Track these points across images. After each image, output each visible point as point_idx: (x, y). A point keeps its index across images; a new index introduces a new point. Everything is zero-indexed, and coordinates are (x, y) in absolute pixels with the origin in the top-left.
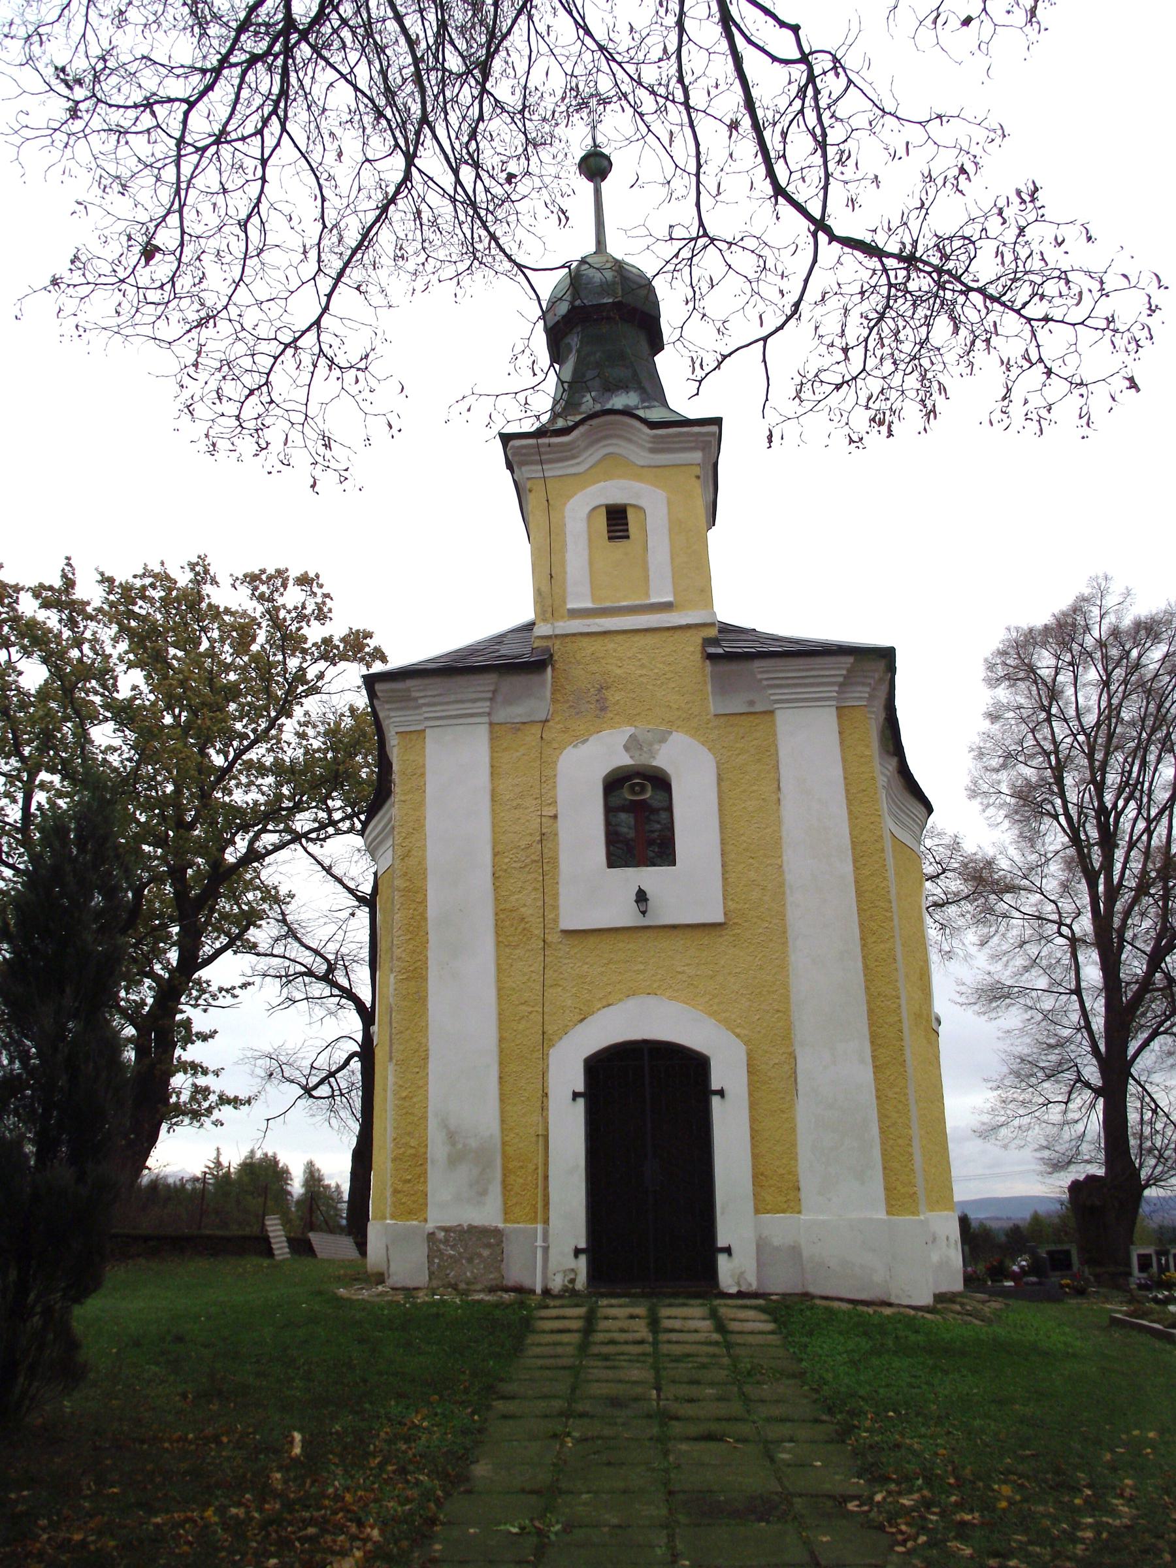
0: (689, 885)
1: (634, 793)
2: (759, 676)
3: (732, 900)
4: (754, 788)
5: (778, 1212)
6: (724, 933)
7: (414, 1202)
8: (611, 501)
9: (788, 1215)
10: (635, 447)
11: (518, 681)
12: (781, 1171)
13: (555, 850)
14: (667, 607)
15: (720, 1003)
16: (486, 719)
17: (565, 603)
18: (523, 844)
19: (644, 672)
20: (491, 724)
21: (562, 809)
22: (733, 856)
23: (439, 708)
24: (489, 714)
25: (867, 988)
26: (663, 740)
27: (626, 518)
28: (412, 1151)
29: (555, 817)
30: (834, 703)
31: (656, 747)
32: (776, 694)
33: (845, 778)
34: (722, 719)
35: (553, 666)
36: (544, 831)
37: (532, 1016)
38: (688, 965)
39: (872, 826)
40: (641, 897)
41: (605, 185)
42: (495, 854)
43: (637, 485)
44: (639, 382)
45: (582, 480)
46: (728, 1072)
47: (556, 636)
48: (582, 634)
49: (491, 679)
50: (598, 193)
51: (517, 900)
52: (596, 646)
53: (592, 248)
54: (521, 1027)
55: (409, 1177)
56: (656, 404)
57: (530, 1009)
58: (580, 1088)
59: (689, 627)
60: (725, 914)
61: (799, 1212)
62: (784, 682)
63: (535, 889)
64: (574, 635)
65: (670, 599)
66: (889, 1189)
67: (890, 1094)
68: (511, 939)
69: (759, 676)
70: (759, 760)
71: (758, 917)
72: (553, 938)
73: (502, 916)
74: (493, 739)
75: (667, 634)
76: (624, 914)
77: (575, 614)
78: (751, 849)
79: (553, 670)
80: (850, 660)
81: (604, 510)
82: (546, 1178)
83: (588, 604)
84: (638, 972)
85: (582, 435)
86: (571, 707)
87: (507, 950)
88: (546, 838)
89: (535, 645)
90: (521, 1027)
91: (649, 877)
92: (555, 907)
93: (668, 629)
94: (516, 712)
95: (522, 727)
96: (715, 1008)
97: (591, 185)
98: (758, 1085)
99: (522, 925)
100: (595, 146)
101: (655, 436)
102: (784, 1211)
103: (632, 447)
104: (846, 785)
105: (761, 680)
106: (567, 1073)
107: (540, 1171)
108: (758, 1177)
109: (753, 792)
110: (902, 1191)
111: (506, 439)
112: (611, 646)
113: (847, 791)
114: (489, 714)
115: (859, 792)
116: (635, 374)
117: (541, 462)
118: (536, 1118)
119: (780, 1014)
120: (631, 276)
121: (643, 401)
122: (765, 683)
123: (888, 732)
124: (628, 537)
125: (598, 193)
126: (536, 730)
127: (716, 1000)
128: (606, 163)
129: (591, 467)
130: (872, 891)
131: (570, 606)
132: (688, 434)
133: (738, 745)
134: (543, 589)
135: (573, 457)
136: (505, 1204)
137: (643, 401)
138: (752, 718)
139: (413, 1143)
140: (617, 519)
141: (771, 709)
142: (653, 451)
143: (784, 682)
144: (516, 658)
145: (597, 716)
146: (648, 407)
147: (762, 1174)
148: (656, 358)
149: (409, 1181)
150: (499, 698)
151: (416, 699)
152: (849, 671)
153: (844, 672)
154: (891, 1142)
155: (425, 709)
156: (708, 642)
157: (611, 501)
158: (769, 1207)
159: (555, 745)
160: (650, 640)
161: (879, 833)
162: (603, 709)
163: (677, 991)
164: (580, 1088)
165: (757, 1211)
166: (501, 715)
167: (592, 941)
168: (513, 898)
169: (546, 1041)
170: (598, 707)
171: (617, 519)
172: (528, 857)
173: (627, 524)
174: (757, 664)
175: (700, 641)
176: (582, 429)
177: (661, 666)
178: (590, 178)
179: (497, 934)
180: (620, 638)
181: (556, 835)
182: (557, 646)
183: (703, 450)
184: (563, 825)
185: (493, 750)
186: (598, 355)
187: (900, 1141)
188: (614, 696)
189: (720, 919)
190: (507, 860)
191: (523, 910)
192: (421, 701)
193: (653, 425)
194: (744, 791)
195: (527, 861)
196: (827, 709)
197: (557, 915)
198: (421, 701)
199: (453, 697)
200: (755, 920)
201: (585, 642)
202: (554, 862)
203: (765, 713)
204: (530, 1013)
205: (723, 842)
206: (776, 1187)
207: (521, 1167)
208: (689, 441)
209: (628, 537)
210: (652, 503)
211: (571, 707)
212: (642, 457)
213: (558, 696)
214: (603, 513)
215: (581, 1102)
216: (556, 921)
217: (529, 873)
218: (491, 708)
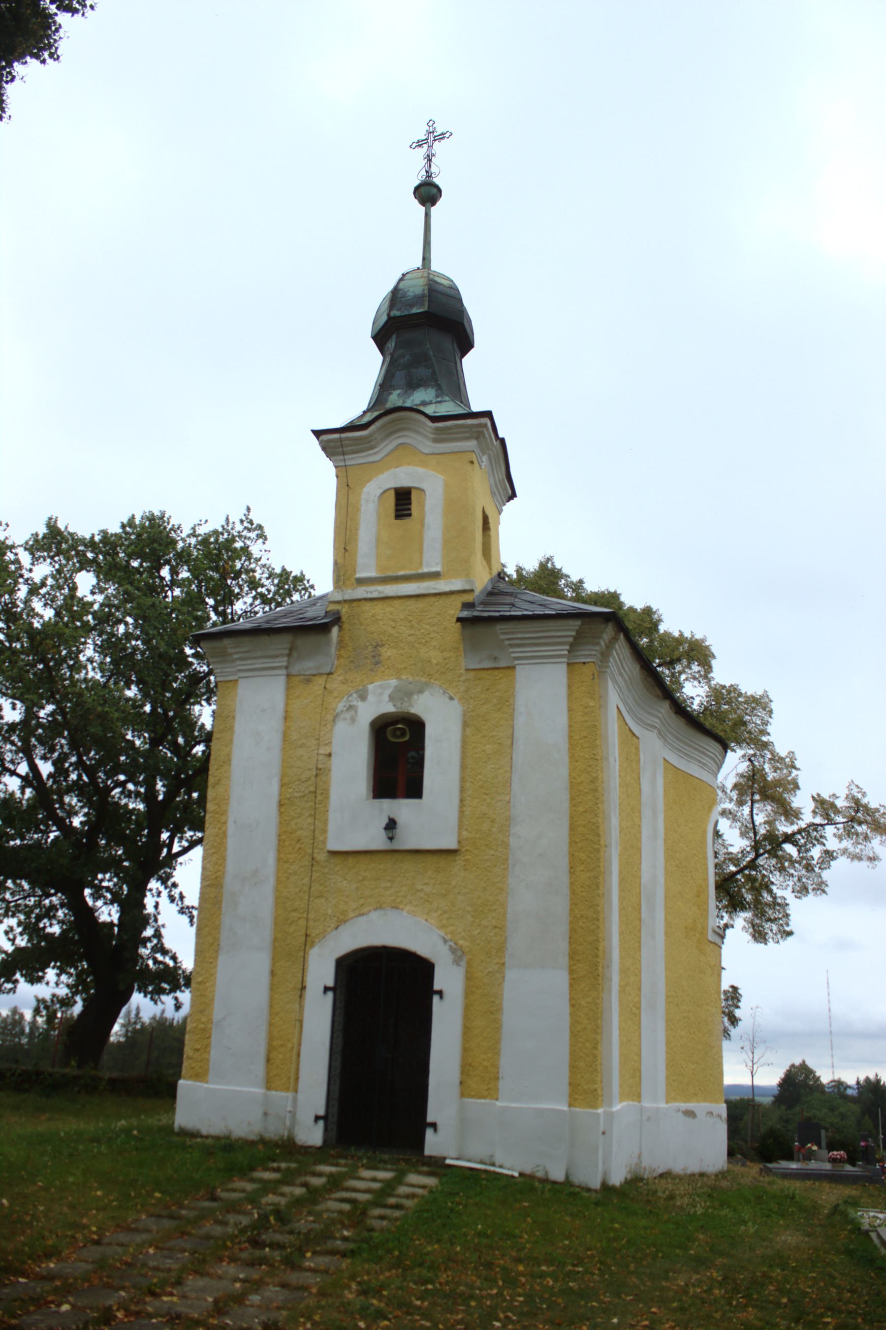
0: (432, 818)
1: (395, 736)
2: (502, 637)
3: (466, 830)
4: (494, 733)
5: (480, 1098)
6: (457, 858)
7: (201, 1067)
8: (399, 485)
9: (487, 1101)
10: (421, 439)
11: (305, 642)
12: (485, 1063)
13: (327, 783)
14: (435, 575)
15: (448, 919)
16: (284, 672)
17: (355, 572)
18: (303, 777)
19: (412, 632)
20: (288, 675)
21: (335, 749)
22: (469, 792)
23: (249, 662)
24: (287, 668)
25: (571, 910)
26: (421, 691)
27: (410, 499)
28: (202, 1026)
29: (330, 755)
30: (566, 660)
31: (415, 697)
32: (517, 652)
33: (570, 726)
34: (472, 674)
35: (340, 627)
36: (320, 766)
37: (300, 922)
38: (426, 884)
39: (589, 769)
40: (391, 825)
41: (433, 209)
42: (282, 785)
43: (421, 470)
44: (436, 381)
45: (377, 467)
46: (448, 978)
47: (345, 601)
48: (366, 599)
49: (285, 641)
50: (427, 216)
51: (296, 824)
52: (378, 609)
53: (419, 263)
54: (291, 930)
55: (198, 1047)
56: (447, 398)
57: (299, 915)
58: (331, 983)
59: (452, 593)
60: (459, 842)
61: (497, 1099)
62: (518, 642)
63: (310, 815)
64: (359, 600)
65: (438, 568)
66: (573, 1085)
67: (583, 1003)
68: (289, 856)
69: (502, 637)
70: (499, 710)
71: (486, 845)
72: (321, 857)
73: (284, 837)
74: (288, 688)
75: (433, 599)
76: (375, 839)
77: (361, 582)
78: (484, 785)
79: (340, 631)
80: (578, 623)
81: (392, 493)
82: (299, 1055)
83: (372, 573)
84: (387, 889)
85: (379, 429)
86: (352, 662)
87: (286, 866)
88: (321, 773)
89: (328, 609)
90: (291, 930)
91: (403, 809)
92: (324, 831)
93: (435, 595)
94: (307, 665)
95: (313, 678)
96: (444, 922)
97: (424, 208)
98: (474, 989)
99: (298, 845)
100: (429, 174)
101: (437, 429)
102: (485, 1097)
103: (420, 438)
104: (570, 732)
105: (503, 640)
106: (321, 971)
107: (295, 1050)
108: (466, 1067)
109: (493, 736)
110: (585, 1087)
111: (318, 433)
112: (389, 609)
113: (570, 737)
114: (287, 668)
115: (581, 739)
116: (434, 373)
117: (344, 454)
118: (297, 1006)
119: (497, 930)
120: (441, 288)
121: (437, 396)
122: (507, 642)
123: (650, 680)
124: (410, 515)
125: (427, 216)
126: (321, 681)
127: (446, 916)
128: (435, 191)
129: (387, 455)
130: (584, 826)
131: (358, 575)
132: (462, 426)
133: (483, 696)
134: (339, 561)
135: (372, 448)
136: (268, 1074)
137: (437, 396)
138: (496, 672)
139: (204, 1019)
140: (403, 501)
141: (509, 664)
142: (436, 441)
143: (518, 642)
144: (311, 620)
145: (371, 670)
146: (440, 402)
147: (470, 1065)
148: (464, 360)
149: (198, 1050)
150: (295, 654)
151: (231, 654)
152: (578, 632)
153: (574, 633)
154: (580, 1044)
155: (238, 663)
156: (467, 606)
157: (398, 485)
158: (473, 1093)
159: (335, 694)
160: (411, 603)
161: (594, 775)
162: (377, 663)
163: (416, 906)
164: (331, 983)
165: (462, 1095)
166: (297, 668)
167: (351, 860)
168: (293, 822)
169: (308, 941)
170: (371, 660)
171: (403, 501)
172: (306, 788)
173: (410, 504)
174: (500, 627)
175: (459, 605)
176: (378, 424)
177: (427, 627)
178: (423, 202)
179: (279, 852)
180: (396, 603)
181: (329, 770)
182: (344, 610)
183: (477, 438)
184: (335, 762)
185: (288, 697)
186: (407, 357)
187: (587, 1044)
188: (387, 652)
189: (452, 845)
190: (290, 790)
191: (300, 832)
192: (235, 656)
193: (434, 419)
194: (484, 736)
195: (302, 794)
196: (559, 665)
197: (326, 838)
198: (235, 656)
199: (259, 654)
200: (483, 848)
201: (367, 606)
202: (326, 793)
203: (508, 668)
204: (299, 918)
205: (463, 780)
206: (480, 1077)
207: (282, 1045)
208: (465, 432)
209: (410, 515)
210: (431, 483)
211: (352, 662)
212: (426, 445)
213: (343, 652)
214: (392, 494)
215: (330, 995)
216: (324, 842)
217: (307, 801)
218: (289, 662)
